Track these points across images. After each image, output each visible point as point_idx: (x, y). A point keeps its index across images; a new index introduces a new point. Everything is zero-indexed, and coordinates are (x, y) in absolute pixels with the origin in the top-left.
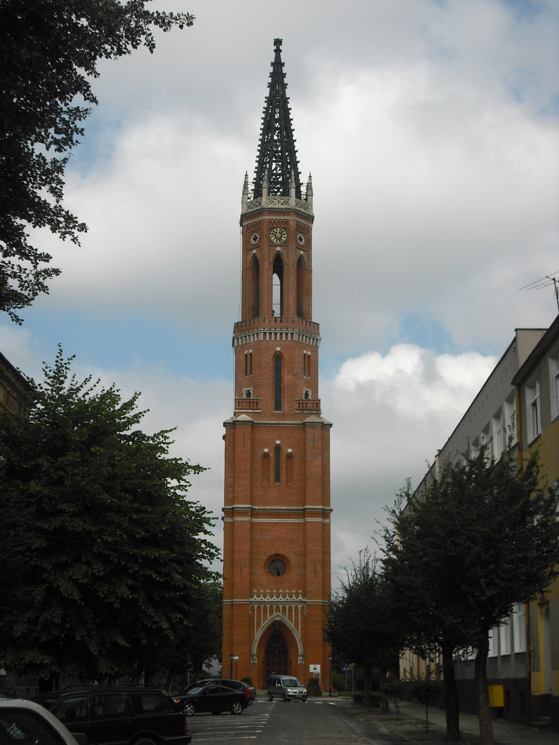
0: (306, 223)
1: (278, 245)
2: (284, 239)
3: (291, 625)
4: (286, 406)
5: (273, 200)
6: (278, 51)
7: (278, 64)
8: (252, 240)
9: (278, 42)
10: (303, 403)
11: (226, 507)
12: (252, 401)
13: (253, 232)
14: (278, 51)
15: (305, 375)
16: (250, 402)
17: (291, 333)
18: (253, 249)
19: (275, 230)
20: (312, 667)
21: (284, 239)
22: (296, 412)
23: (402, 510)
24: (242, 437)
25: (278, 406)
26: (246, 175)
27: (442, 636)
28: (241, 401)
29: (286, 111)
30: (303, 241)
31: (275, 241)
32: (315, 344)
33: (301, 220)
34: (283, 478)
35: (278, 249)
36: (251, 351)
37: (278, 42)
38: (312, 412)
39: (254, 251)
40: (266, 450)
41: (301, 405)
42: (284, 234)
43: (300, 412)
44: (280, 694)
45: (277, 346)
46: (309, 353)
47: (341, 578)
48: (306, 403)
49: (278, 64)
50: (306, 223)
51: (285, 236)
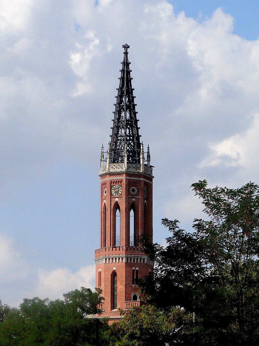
0: (148, 181)
2: (120, 192)
5: (118, 166)
6: (126, 53)
7: (126, 64)
9: (126, 47)
14: (126, 53)
15: (133, 283)
16: (127, 304)
21: (120, 192)
23: (118, 211)
29: (131, 99)
31: (114, 195)
33: (146, 180)
35: (117, 199)
36: (137, 269)
37: (126, 47)
41: (130, 305)
44: (100, 284)
47: (75, 95)
49: (126, 64)
50: (148, 181)
51: (121, 190)
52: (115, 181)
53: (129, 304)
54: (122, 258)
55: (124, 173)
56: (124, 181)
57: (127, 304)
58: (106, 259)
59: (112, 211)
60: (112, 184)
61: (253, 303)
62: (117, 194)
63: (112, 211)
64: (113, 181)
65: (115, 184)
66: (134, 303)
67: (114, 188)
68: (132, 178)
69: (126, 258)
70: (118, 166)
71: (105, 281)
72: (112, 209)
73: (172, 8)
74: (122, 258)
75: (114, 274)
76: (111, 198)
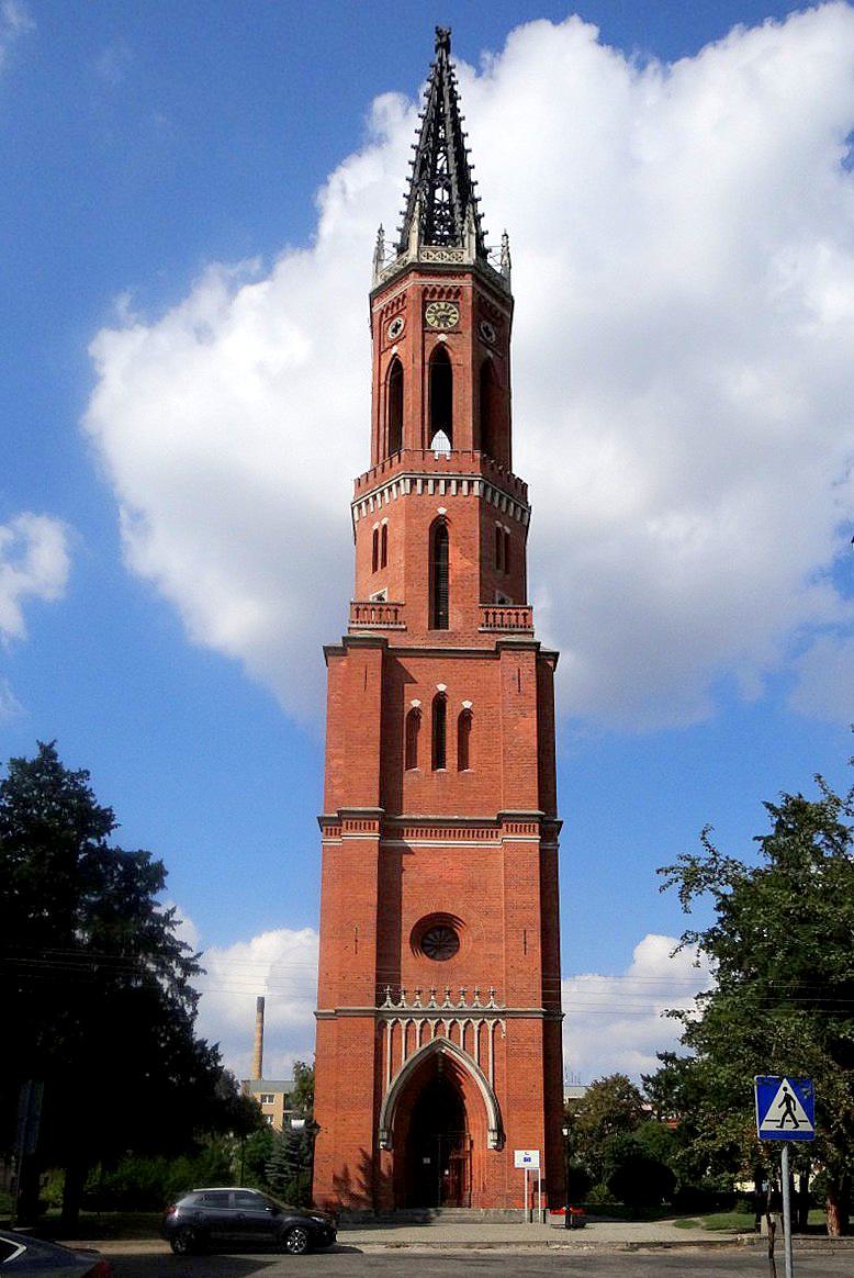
1: (442, 332)
3: (468, 1064)
4: (455, 618)
5: (431, 253)
8: (390, 333)
9: (686, 911)
10: (494, 614)
11: (321, 1011)
12: (385, 608)
13: (392, 318)
16: (381, 610)
17: (469, 481)
18: (391, 347)
19: (435, 305)
20: (519, 1155)
22: (481, 629)
24: (363, 671)
25: (438, 620)
26: (381, 231)
27: (85, 928)
28: (361, 607)
30: (494, 336)
32: (519, 516)
34: (452, 757)
35: (442, 337)
36: (384, 521)
38: (516, 630)
39: (395, 350)
40: (416, 703)
41: (498, 616)
42: (455, 313)
43: (385, 626)
45: (440, 505)
46: (508, 530)
48: (502, 614)
52: (438, 289)
53: (494, 614)
54: (471, 484)
55: (468, 272)
56: (469, 292)
57: (487, 613)
58: (413, 482)
59: (427, 367)
60: (427, 298)
61: (767, 940)
62: (442, 325)
63: (427, 367)
64: (430, 289)
65: (436, 298)
66: (513, 612)
67: (445, 325)
68: (494, 302)
69: (482, 486)
70: (431, 253)
71: (409, 557)
72: (427, 360)
73: (591, 31)
74: (471, 484)
75: (439, 530)
76: (423, 332)
